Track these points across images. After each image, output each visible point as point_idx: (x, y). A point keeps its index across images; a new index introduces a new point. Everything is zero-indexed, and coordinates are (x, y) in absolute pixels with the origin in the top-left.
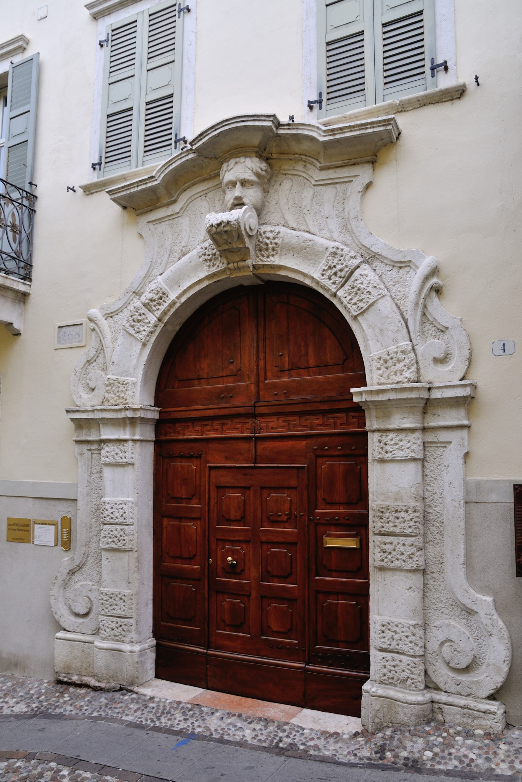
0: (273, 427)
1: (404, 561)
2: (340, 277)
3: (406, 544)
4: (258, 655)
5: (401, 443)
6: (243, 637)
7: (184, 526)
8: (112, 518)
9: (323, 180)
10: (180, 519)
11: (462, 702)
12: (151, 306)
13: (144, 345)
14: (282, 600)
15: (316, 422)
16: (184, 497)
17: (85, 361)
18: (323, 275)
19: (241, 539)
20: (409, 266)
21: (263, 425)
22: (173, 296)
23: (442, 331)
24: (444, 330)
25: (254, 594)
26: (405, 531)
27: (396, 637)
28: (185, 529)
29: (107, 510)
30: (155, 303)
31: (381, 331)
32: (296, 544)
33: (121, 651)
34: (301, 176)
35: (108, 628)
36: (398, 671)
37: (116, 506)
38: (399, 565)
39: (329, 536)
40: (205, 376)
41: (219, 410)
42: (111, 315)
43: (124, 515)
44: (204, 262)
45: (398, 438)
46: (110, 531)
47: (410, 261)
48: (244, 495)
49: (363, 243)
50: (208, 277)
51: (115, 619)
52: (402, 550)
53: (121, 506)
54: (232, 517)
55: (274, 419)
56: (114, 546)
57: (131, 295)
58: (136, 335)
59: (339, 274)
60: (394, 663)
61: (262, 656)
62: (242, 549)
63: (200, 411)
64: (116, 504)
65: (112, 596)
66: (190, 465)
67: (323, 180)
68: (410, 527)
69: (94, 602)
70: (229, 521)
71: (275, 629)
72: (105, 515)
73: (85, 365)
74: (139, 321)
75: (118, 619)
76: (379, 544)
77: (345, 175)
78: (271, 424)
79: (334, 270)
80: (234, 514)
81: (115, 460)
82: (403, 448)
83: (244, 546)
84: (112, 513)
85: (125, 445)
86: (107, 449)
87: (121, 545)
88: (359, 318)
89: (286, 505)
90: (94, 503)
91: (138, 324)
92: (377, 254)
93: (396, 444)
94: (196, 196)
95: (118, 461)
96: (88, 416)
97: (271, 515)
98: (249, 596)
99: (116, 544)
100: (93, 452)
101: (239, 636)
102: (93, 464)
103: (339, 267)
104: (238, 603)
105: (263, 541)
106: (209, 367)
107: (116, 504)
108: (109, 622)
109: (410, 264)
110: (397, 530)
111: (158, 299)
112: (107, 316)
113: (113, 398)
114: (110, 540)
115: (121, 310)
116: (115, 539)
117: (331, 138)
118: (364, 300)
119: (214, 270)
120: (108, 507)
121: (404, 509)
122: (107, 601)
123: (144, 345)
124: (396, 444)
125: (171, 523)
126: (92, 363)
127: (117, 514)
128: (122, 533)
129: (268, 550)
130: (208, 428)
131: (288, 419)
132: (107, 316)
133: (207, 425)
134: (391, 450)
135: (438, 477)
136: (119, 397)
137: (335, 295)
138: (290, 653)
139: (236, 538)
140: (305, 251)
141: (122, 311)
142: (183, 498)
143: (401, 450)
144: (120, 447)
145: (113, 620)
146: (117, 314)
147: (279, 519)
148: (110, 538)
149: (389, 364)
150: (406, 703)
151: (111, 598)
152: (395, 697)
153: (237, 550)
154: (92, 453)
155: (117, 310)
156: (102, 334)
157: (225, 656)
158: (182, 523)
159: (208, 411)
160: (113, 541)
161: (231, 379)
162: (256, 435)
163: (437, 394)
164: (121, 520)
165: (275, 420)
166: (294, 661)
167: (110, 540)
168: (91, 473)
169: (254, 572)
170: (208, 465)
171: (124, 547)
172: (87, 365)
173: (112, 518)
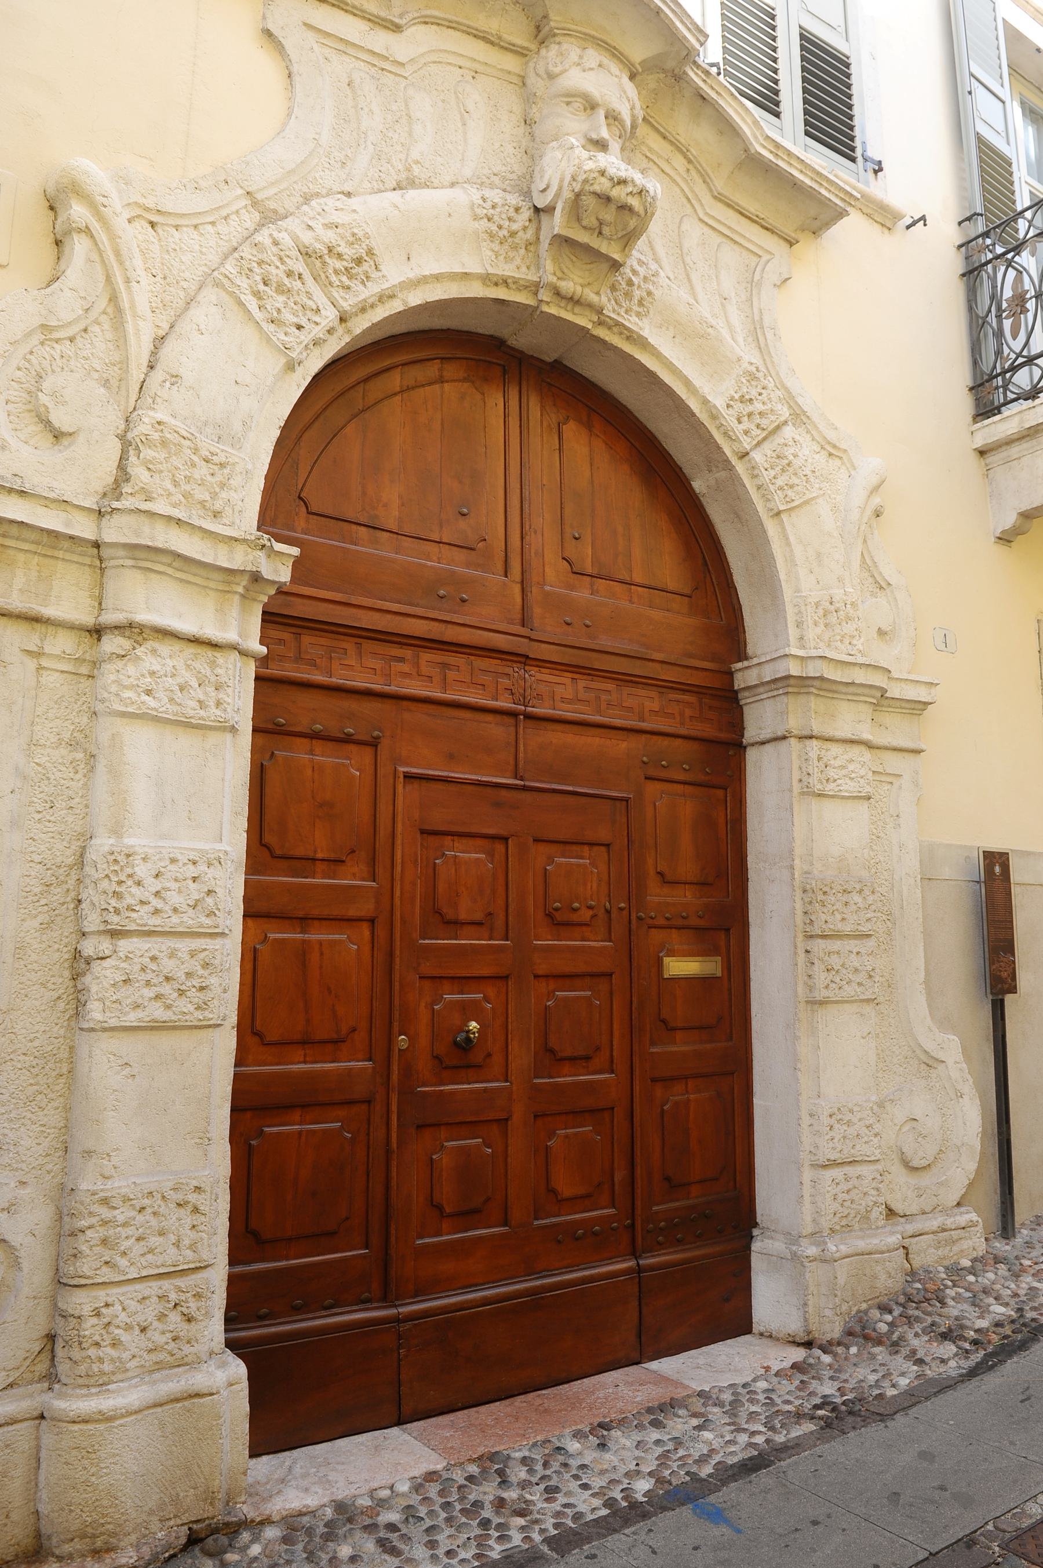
0: (561, 694)
1: (860, 984)
2: (758, 426)
3: (863, 951)
4: (531, 1272)
5: (851, 767)
6: (492, 1236)
7: (320, 943)
8: (157, 912)
9: (719, 221)
10: (304, 921)
11: (934, 1223)
12: (324, 263)
13: (291, 366)
14: (577, 1114)
15: (649, 705)
16: (320, 855)
17: (37, 322)
18: (728, 406)
19: (486, 972)
20: (841, 458)
21: (542, 688)
22: (393, 273)
23: (881, 588)
24: (884, 585)
25: (519, 1113)
26: (860, 928)
27: (851, 1131)
28: (322, 954)
29: (139, 883)
30: (339, 265)
31: (819, 555)
32: (610, 975)
33: (198, 1395)
34: (678, 185)
35: (128, 1328)
36: (856, 1198)
37: (171, 867)
38: (853, 993)
39: (671, 953)
40: (393, 526)
41: (443, 626)
42: (155, 218)
43: (210, 901)
44: (486, 236)
45: (845, 757)
46: (146, 960)
47: (846, 450)
48: (491, 854)
49: (785, 381)
50: (487, 279)
51: (153, 1288)
52: (856, 964)
53: (191, 871)
54: (463, 916)
55: (566, 678)
56: (159, 1013)
57: (237, 198)
58: (265, 325)
59: (757, 419)
60: (850, 1185)
61: (549, 1271)
62: (486, 999)
63: (389, 617)
64: (173, 861)
65: (146, 1202)
66: (343, 764)
67: (719, 221)
68: (868, 920)
69: (22, 1253)
70: (453, 925)
71: (567, 1192)
72: (129, 900)
73: (28, 335)
74: (281, 289)
75: (166, 1284)
76: (822, 954)
77: (753, 238)
78: (559, 690)
79: (750, 408)
80: (466, 909)
81: (176, 708)
82: (853, 775)
83: (491, 991)
84: (157, 894)
85: (221, 661)
86: (150, 663)
87: (191, 1008)
88: (784, 516)
89: (589, 885)
90: (37, 858)
91: (281, 299)
92: (804, 412)
93: (843, 767)
94: (451, 59)
95: (191, 713)
96: (68, 524)
97: (557, 909)
98: (504, 1122)
99: (168, 1007)
100: (45, 663)
101: (480, 1238)
102: (40, 710)
103: (758, 406)
104: (477, 1146)
105: (540, 972)
106: (403, 505)
107: (173, 861)
108: (133, 1305)
109: (844, 457)
110: (847, 928)
111: (353, 260)
112: (139, 212)
113: (170, 494)
114: (148, 993)
115: (195, 221)
116: (167, 989)
117: (771, 157)
118: (796, 488)
119: (507, 270)
120: (142, 871)
121: (858, 887)
122: (125, 1225)
123: (291, 366)
124: (843, 767)
125: (272, 936)
126: (57, 341)
127: (175, 899)
128: (194, 965)
129: (550, 995)
130: (405, 668)
131: (594, 685)
132: (139, 211)
133: (401, 660)
134: (836, 777)
135: (882, 835)
136: (187, 495)
137: (744, 455)
138: (595, 1242)
139: (476, 973)
140: (698, 338)
141: (196, 227)
142: (314, 860)
143: (852, 779)
144: (197, 665)
145: (147, 1293)
146: (177, 227)
147: (574, 918)
148: (148, 983)
149: (833, 619)
150: (889, 1251)
151: (142, 1209)
152: (869, 1248)
153: (474, 1002)
154: (40, 668)
155: (183, 216)
156: (121, 263)
157: (416, 1312)
158: (313, 937)
159: (413, 620)
160: (158, 997)
161: (460, 555)
162: (529, 709)
163: (895, 691)
164: (190, 920)
165: (568, 681)
166: (610, 1259)
167: (148, 993)
168: (33, 743)
169: (521, 1056)
170: (402, 769)
171: (199, 1015)
172: (35, 340)
173: (157, 912)
